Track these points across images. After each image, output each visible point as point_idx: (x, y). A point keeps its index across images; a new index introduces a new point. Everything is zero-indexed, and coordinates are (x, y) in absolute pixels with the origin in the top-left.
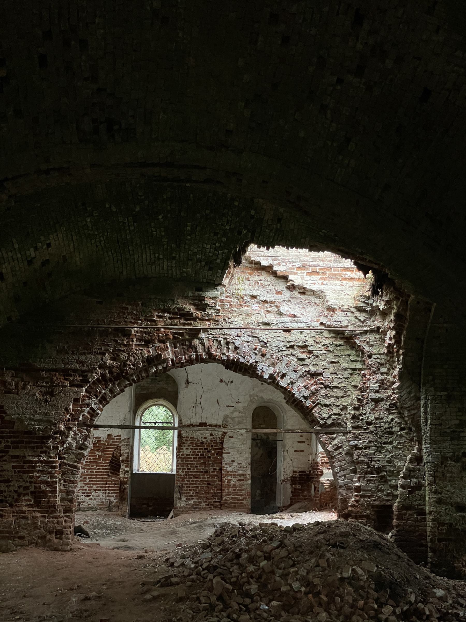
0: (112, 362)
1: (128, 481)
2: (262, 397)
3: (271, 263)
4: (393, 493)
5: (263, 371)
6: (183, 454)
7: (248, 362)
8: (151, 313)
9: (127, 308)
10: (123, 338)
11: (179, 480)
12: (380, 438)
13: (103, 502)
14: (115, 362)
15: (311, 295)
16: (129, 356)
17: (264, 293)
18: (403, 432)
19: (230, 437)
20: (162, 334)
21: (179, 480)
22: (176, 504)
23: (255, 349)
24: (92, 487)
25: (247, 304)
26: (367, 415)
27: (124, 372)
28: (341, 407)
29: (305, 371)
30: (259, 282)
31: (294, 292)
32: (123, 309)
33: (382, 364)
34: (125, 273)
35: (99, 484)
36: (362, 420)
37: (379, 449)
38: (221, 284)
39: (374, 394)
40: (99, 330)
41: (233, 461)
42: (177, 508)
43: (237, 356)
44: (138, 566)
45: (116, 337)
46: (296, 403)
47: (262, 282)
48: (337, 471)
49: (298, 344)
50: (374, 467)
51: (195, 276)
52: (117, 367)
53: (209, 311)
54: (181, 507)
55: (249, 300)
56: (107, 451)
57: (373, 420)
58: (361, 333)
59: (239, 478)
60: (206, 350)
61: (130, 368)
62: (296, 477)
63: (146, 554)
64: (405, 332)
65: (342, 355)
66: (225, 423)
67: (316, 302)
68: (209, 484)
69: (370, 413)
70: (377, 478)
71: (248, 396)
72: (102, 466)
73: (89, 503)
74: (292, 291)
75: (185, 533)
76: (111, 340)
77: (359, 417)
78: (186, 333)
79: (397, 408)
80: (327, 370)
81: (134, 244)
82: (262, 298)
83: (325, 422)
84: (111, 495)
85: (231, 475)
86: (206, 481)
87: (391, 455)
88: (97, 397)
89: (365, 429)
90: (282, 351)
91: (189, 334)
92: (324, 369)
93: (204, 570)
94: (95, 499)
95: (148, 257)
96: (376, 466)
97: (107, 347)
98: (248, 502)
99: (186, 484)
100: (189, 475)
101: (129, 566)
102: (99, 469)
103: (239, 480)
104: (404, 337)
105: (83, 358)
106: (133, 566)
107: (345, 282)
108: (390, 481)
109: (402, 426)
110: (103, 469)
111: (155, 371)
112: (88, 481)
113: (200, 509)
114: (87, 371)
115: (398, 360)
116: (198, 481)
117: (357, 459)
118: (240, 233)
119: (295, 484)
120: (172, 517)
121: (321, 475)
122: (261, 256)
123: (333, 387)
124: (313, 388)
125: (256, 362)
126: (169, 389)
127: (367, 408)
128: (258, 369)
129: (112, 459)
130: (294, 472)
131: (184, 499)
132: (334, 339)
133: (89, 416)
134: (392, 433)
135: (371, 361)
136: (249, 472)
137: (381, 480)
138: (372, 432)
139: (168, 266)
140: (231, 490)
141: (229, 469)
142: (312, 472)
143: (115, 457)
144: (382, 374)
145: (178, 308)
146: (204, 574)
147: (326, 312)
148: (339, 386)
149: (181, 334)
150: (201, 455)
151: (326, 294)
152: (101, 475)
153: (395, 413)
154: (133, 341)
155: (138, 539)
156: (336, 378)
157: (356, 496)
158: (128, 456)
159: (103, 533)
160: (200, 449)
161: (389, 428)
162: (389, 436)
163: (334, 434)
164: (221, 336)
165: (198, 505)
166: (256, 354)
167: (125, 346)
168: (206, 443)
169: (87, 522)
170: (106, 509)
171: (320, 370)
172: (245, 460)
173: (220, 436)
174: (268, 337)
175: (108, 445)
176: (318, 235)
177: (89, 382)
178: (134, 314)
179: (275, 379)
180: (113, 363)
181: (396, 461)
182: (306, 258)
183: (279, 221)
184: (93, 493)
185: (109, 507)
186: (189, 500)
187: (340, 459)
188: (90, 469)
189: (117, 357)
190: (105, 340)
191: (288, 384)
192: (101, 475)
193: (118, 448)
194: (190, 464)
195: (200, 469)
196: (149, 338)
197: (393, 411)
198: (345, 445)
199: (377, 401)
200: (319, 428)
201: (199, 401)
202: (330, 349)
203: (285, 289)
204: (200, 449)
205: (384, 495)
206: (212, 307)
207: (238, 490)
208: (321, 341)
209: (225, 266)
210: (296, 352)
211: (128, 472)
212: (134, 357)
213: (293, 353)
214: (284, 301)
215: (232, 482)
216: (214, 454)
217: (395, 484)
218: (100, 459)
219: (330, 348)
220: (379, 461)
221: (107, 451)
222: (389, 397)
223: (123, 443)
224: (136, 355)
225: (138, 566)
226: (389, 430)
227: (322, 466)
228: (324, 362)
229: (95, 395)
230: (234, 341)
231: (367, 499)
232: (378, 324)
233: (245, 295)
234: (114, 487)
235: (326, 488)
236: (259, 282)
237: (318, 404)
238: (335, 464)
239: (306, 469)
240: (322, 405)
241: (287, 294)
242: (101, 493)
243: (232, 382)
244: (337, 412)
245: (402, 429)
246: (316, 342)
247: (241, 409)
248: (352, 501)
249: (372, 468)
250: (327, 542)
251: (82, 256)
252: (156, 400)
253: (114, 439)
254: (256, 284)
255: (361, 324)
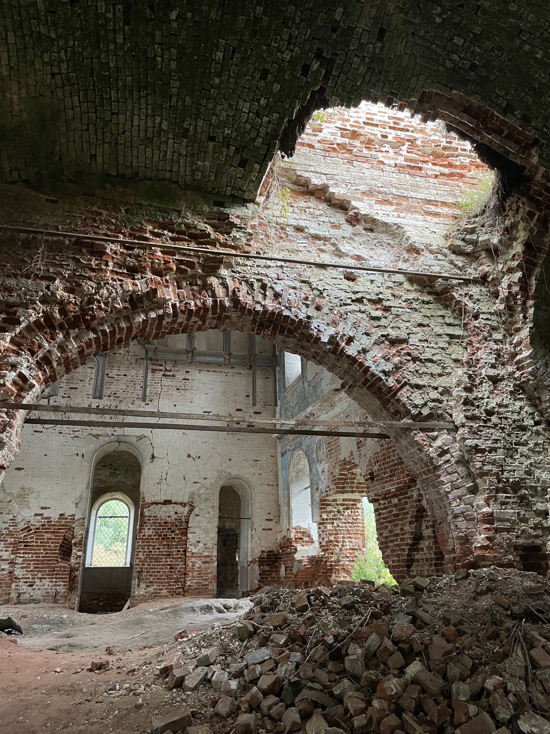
0: (66, 294)
1: (79, 567)
2: (229, 473)
3: (326, 182)
4: (542, 524)
5: (319, 331)
6: (144, 535)
7: (296, 316)
8: (142, 224)
9: (100, 214)
10: (89, 257)
11: (139, 565)
12: (509, 435)
13: (48, 593)
14: (71, 296)
15: (382, 232)
16: (99, 287)
17: (314, 225)
18: (540, 428)
19: (196, 515)
20: (158, 260)
21: (139, 565)
22: (134, 593)
23: (306, 299)
24: (36, 575)
25: (289, 238)
26: (486, 400)
27: (87, 314)
28: (440, 389)
29: (382, 336)
30: (307, 210)
31: (358, 227)
32: (92, 214)
33: (494, 329)
34: (99, 159)
35: (46, 571)
36: (478, 407)
37: (510, 452)
38: (253, 201)
39: (490, 370)
40: (47, 241)
41: (199, 542)
42: (134, 596)
43: (279, 306)
44: (92, 689)
45: (78, 254)
46: (369, 384)
47: (311, 210)
48: (447, 490)
49: (368, 297)
50: (508, 481)
51: (216, 179)
52: (76, 304)
53: (235, 233)
54: (139, 596)
55: (293, 233)
56: (58, 532)
57: (494, 408)
58: (460, 284)
59: (204, 560)
60: (230, 294)
61: (100, 308)
62: (264, 558)
63: (110, 658)
64: (538, 270)
65: (432, 316)
66: (191, 500)
67: (389, 241)
68: (172, 568)
69: (488, 397)
70: (514, 500)
71: (215, 472)
72: (50, 550)
73: (31, 594)
74: (354, 226)
75: (155, 622)
76: (68, 257)
77: (475, 402)
78: (198, 263)
79: (524, 392)
80: (414, 335)
81: (120, 84)
82: (312, 231)
83: (420, 412)
84: (58, 583)
85: (196, 557)
86: (169, 565)
87: (529, 462)
88: (33, 353)
89: (485, 422)
90: (346, 305)
91: (203, 267)
92: (408, 334)
93: (265, 693)
94: (39, 589)
95: (143, 123)
96: (511, 480)
97: (60, 269)
98: (213, 587)
99: (146, 568)
100: (150, 559)
101: (72, 690)
102: (46, 553)
103: (204, 562)
104: (536, 280)
105: (12, 282)
106: (81, 691)
107: (428, 218)
108: (535, 504)
109: (537, 418)
110: (51, 553)
111: (143, 320)
112: (32, 568)
113: (161, 597)
114: (18, 306)
115: (525, 318)
116: (159, 565)
117: (480, 468)
118: (306, 69)
119: (263, 565)
120: (129, 608)
121: (295, 553)
122: (311, 172)
123: (425, 360)
124: (396, 360)
125: (309, 317)
126: (128, 483)
127: (484, 389)
128: (313, 327)
129: (63, 542)
130: (263, 552)
131: (143, 585)
132: (419, 293)
133: (14, 389)
134: (524, 429)
135: (479, 323)
136: (215, 554)
137: (521, 502)
138: (496, 425)
139: (174, 152)
140: (195, 574)
141: (194, 551)
142: (280, 551)
143: (67, 540)
144: (496, 342)
145: (186, 224)
146: (270, 708)
147: (406, 256)
148: (434, 358)
149: (191, 265)
150: (164, 535)
151: (405, 229)
152: (49, 560)
153: (523, 398)
154: (107, 265)
155: (89, 634)
156: (428, 347)
157: (489, 529)
158: (82, 538)
159: (43, 629)
160: (163, 529)
161: (519, 421)
162: (521, 433)
163: (433, 430)
164: (253, 277)
165: (159, 593)
166: (307, 306)
167: (93, 270)
168: (170, 523)
169: (25, 617)
170: (51, 601)
171: (404, 336)
172: (211, 540)
173: (185, 514)
174: (324, 284)
175: (59, 525)
176: (442, 69)
177: (19, 323)
178: (112, 223)
179: (338, 344)
180: (69, 296)
181: (537, 473)
182: (373, 182)
183: (382, 33)
184: (38, 582)
185: (55, 598)
186: (148, 586)
187: (449, 470)
188: (36, 553)
189: (77, 288)
190: (57, 258)
191: (359, 352)
192: (49, 560)
193: (71, 529)
194: (151, 545)
195: (162, 552)
196: (137, 264)
197: (520, 396)
198: (454, 448)
199: (495, 380)
200: (410, 421)
201: (164, 477)
202: (415, 306)
203: (344, 222)
204: (163, 529)
205: (531, 528)
206: (241, 228)
207: (203, 574)
208: (401, 294)
209: (268, 156)
210: (366, 307)
211: (80, 557)
212: (108, 290)
213: (362, 309)
214: (344, 238)
215: (197, 565)
216: (178, 534)
217: (543, 508)
218: (48, 543)
219: (414, 305)
220: (514, 471)
221: (58, 532)
222: (511, 374)
223: (77, 523)
224: (113, 287)
225: (92, 689)
226: (519, 424)
227: (296, 542)
228: (408, 324)
229: (29, 350)
230: (274, 286)
231: (505, 535)
232: (487, 269)
233: (288, 225)
234: (62, 574)
235: (305, 565)
236: (307, 210)
237: (405, 384)
238: (442, 479)
239: (275, 549)
240: (412, 386)
241: (348, 230)
242: (46, 582)
243: (199, 457)
244: (436, 397)
245: (537, 423)
246: (394, 296)
247: (208, 486)
248: (480, 539)
249: (505, 482)
250: (507, 610)
251: (23, 93)
252: (113, 493)
253: (67, 519)
254: (303, 212)
255: (459, 272)
